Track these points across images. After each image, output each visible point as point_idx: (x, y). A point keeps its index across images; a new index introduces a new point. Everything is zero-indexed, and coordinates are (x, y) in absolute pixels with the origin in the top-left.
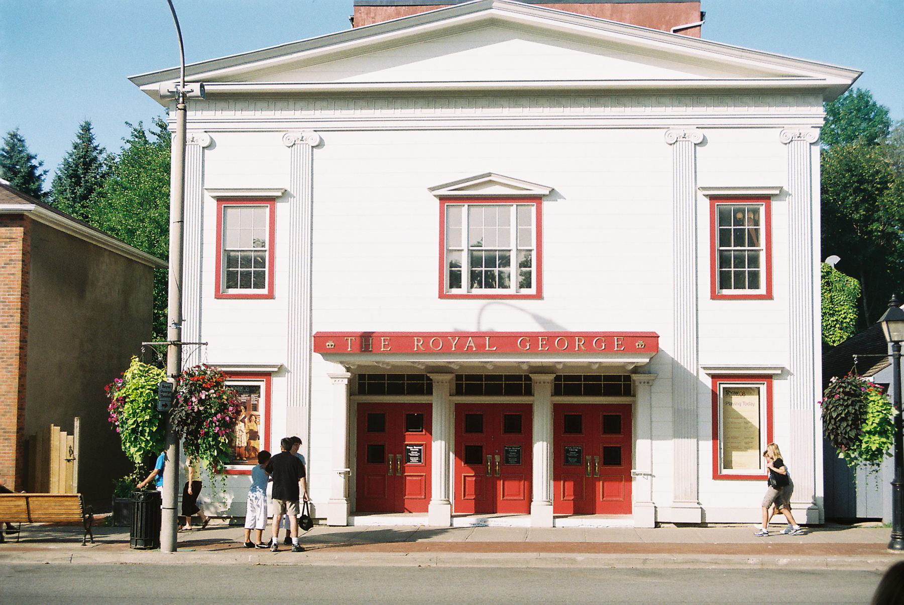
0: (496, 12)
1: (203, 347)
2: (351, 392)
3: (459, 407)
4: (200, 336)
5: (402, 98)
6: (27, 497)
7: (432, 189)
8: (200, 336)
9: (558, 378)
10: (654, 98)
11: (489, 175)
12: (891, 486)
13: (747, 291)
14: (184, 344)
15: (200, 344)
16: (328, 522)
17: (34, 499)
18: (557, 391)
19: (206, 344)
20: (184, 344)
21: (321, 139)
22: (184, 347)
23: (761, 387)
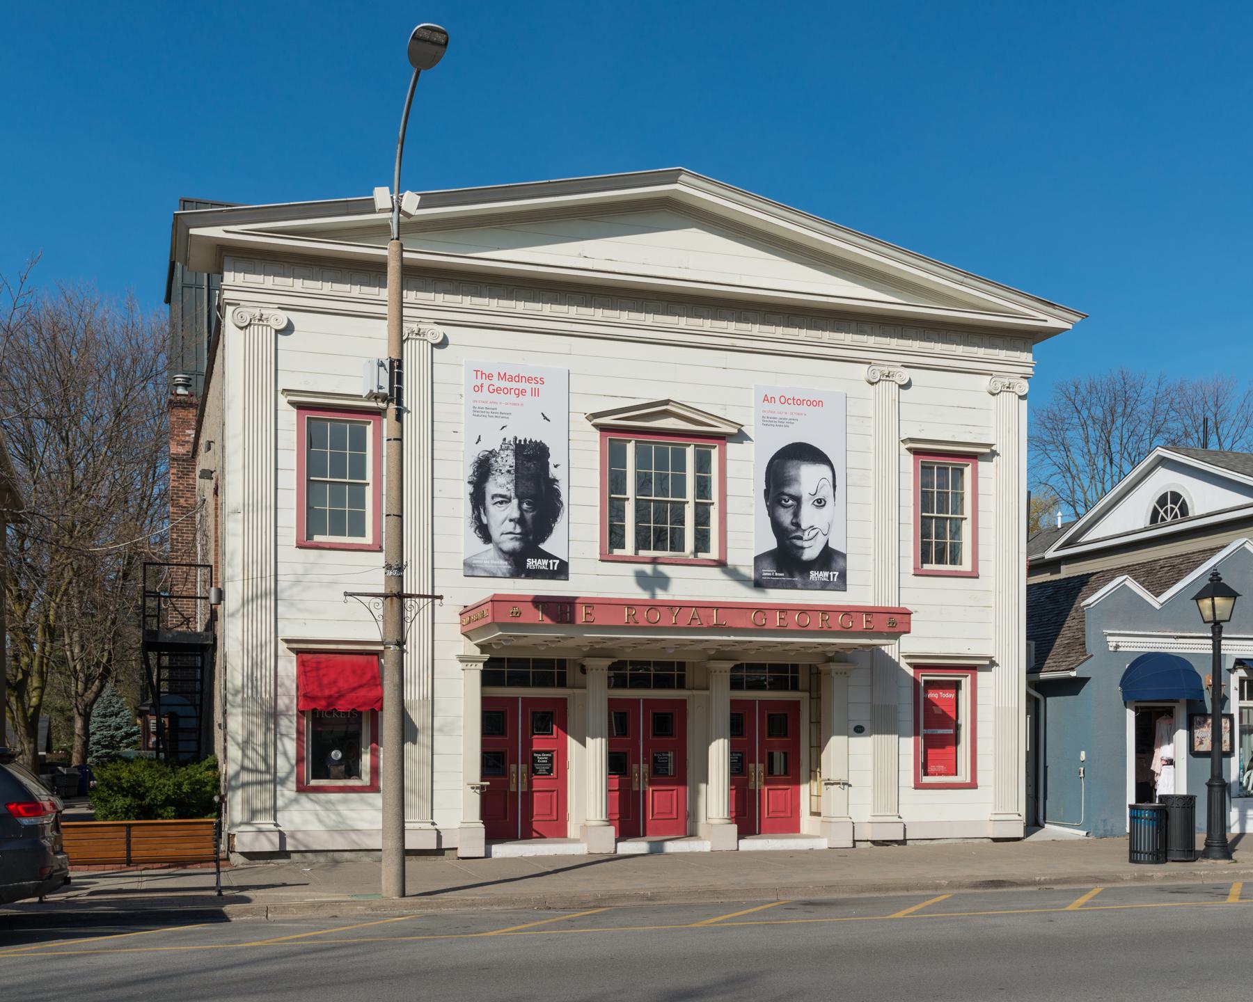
0: (689, 188)
1: (437, 601)
2: (488, 678)
3: (612, 703)
4: (433, 587)
5: (551, 290)
6: (129, 826)
7: (596, 415)
8: (433, 587)
9: (737, 668)
10: (854, 325)
11: (667, 402)
12: (1206, 788)
13: (948, 567)
14: (410, 596)
15: (433, 597)
16: (461, 853)
17: (71, 830)
18: (736, 684)
19: (441, 597)
20: (410, 596)
21: (445, 337)
22: (408, 602)
23: (963, 680)
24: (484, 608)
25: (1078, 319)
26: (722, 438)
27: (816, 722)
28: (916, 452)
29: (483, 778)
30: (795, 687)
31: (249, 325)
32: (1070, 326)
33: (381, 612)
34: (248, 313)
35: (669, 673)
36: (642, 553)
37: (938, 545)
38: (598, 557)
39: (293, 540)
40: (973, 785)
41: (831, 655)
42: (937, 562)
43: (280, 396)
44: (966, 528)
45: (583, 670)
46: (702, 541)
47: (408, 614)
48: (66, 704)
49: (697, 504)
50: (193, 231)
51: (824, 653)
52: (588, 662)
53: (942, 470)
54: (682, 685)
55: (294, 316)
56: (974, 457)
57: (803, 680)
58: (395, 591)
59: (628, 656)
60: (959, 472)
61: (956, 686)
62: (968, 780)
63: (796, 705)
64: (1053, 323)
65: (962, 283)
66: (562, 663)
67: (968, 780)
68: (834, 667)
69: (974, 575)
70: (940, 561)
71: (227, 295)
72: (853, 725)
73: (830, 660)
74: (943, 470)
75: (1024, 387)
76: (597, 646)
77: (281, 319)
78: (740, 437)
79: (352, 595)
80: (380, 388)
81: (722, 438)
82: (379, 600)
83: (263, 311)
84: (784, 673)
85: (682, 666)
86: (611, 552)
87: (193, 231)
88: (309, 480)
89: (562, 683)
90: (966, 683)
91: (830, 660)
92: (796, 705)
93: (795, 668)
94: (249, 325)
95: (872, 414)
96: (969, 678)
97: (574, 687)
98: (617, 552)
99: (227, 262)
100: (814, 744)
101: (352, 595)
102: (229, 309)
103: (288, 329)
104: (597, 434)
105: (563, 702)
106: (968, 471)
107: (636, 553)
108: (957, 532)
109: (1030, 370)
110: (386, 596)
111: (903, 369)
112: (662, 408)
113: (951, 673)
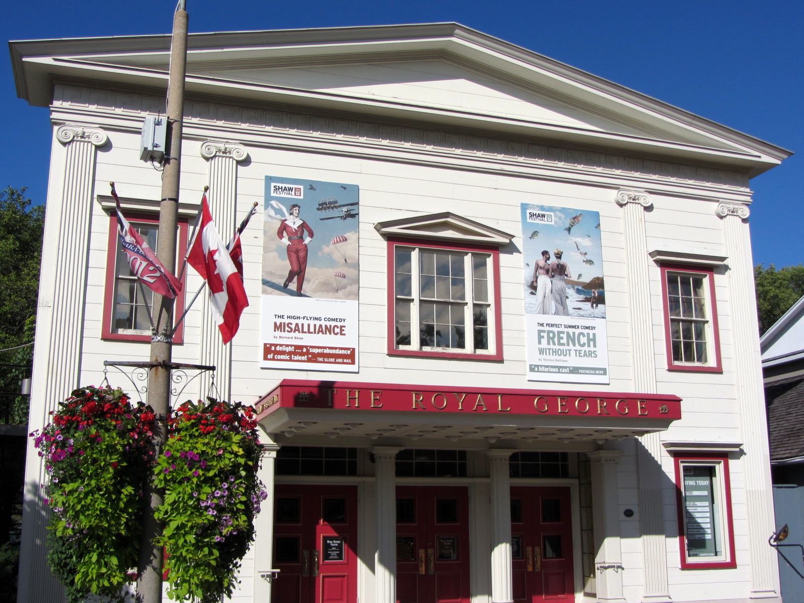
9: (514, 457)
11: (447, 215)
13: (696, 364)
24: (274, 395)
25: (785, 157)
26: (496, 248)
27: (588, 506)
28: (662, 264)
29: (274, 567)
30: (565, 475)
31: (72, 141)
32: (779, 162)
33: (145, 383)
34: (70, 131)
35: (451, 461)
36: (426, 349)
37: (686, 345)
38: (386, 351)
39: (99, 333)
40: (732, 565)
41: (601, 443)
42: (686, 360)
43: (95, 201)
44: (709, 330)
45: (372, 458)
46: (480, 340)
47: (173, 386)
48: (53, 505)
49: (475, 305)
50: (24, 59)
51: (594, 442)
52: (378, 451)
53: (684, 276)
54: (463, 473)
55: (113, 136)
56: (710, 269)
57: (572, 466)
58: (160, 360)
59: (415, 445)
60: (698, 284)
61: (710, 472)
62: (728, 560)
63: (566, 491)
64: (766, 159)
65: (690, 124)
66: (353, 452)
67: (728, 560)
68: (603, 454)
69: (718, 371)
70: (689, 358)
71: (54, 115)
72: (623, 509)
73: (599, 448)
74: (685, 282)
75: (746, 212)
76: (386, 434)
77: (101, 136)
78: (510, 248)
79: (113, 364)
80: (156, 146)
81: (496, 248)
82: (144, 371)
83: (85, 130)
84: (551, 462)
85: (463, 454)
86: (397, 348)
87: (24, 59)
88: (117, 279)
89: (353, 472)
90: (720, 468)
91: (599, 448)
92: (566, 491)
93: (564, 456)
94: (72, 141)
95: (622, 231)
96: (722, 465)
97: (364, 476)
98: (402, 347)
99: (57, 91)
100: (585, 527)
101: (113, 364)
102: (56, 128)
103: (106, 146)
104: (384, 244)
105: (352, 491)
106: (706, 281)
107: (421, 349)
108: (700, 334)
109: (748, 199)
110: (150, 366)
111: (647, 195)
112: (442, 220)
113: (703, 460)
